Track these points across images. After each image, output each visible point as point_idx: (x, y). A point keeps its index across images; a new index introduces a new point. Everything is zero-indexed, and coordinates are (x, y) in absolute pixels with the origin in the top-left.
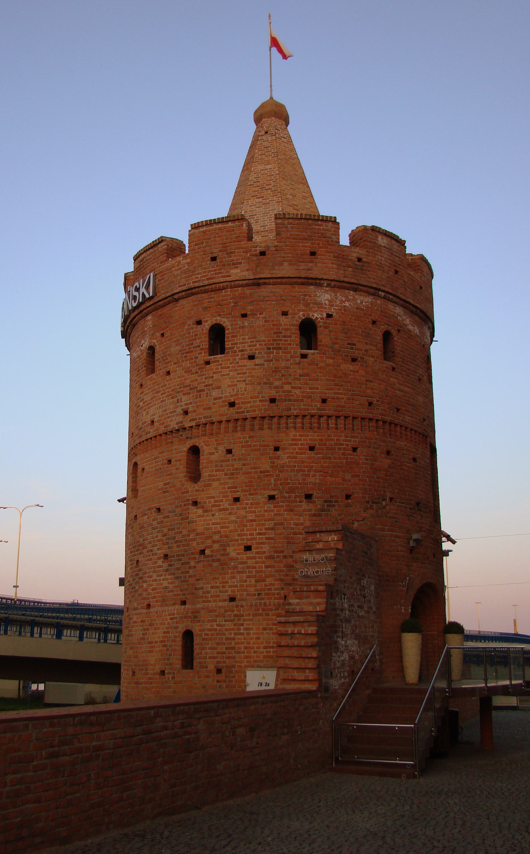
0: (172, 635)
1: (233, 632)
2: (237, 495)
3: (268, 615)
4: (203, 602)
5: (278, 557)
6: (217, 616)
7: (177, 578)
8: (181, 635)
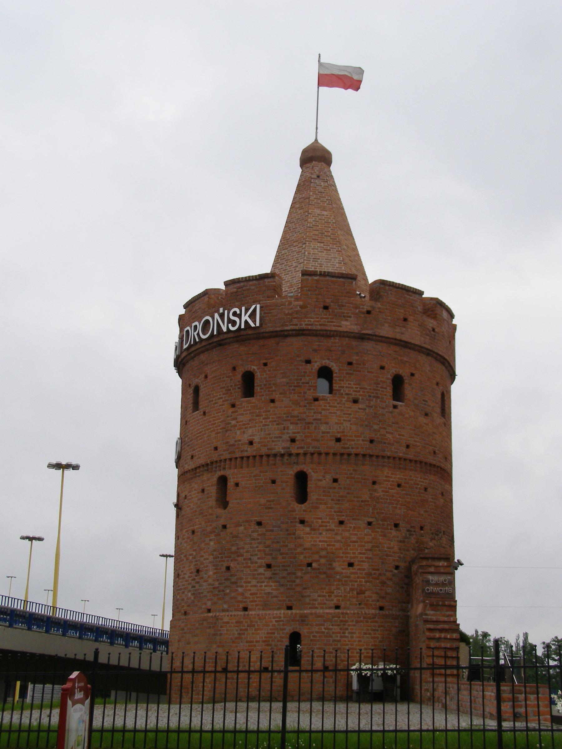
0: (278, 636)
1: (339, 635)
2: (341, 519)
3: (367, 622)
4: (311, 608)
5: (375, 574)
6: (324, 621)
7: (283, 585)
8: (288, 636)
